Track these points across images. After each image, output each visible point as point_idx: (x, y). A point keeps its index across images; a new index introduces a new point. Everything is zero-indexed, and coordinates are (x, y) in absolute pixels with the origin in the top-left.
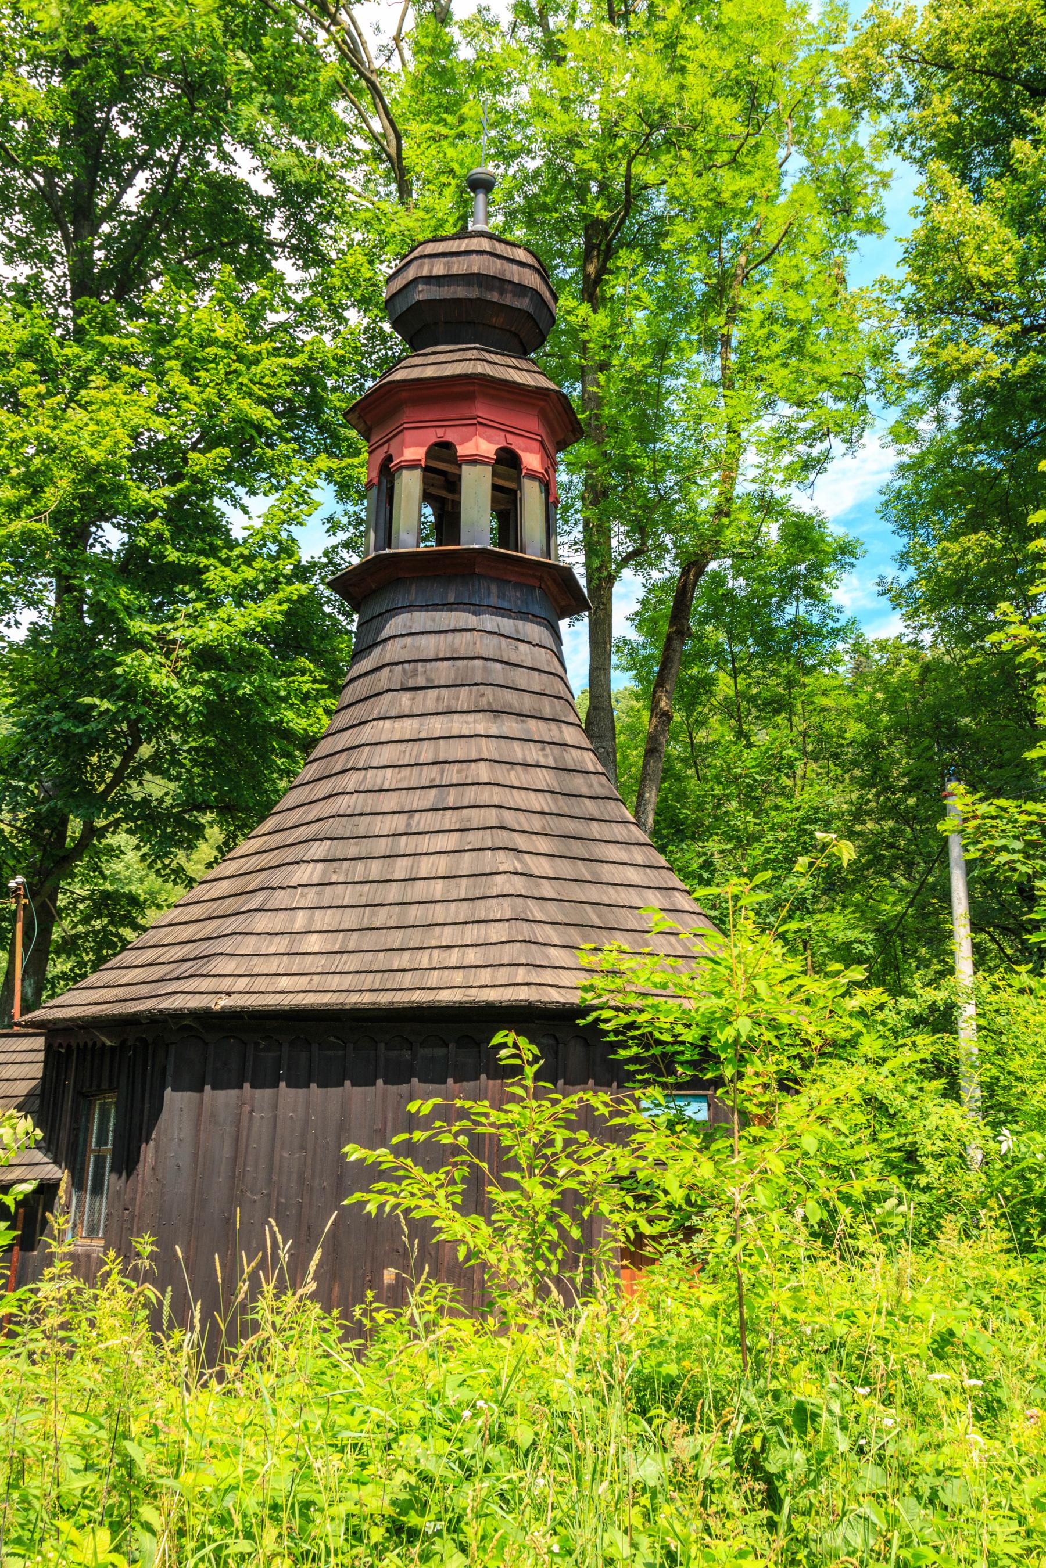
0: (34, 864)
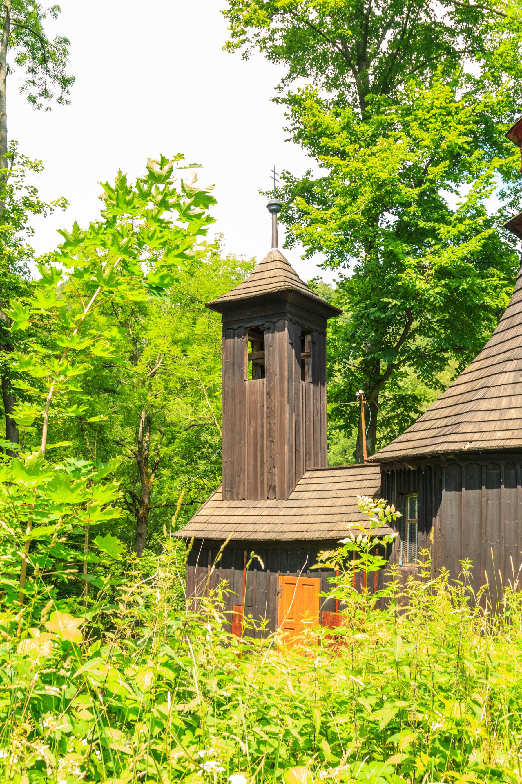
0: (366, 384)
